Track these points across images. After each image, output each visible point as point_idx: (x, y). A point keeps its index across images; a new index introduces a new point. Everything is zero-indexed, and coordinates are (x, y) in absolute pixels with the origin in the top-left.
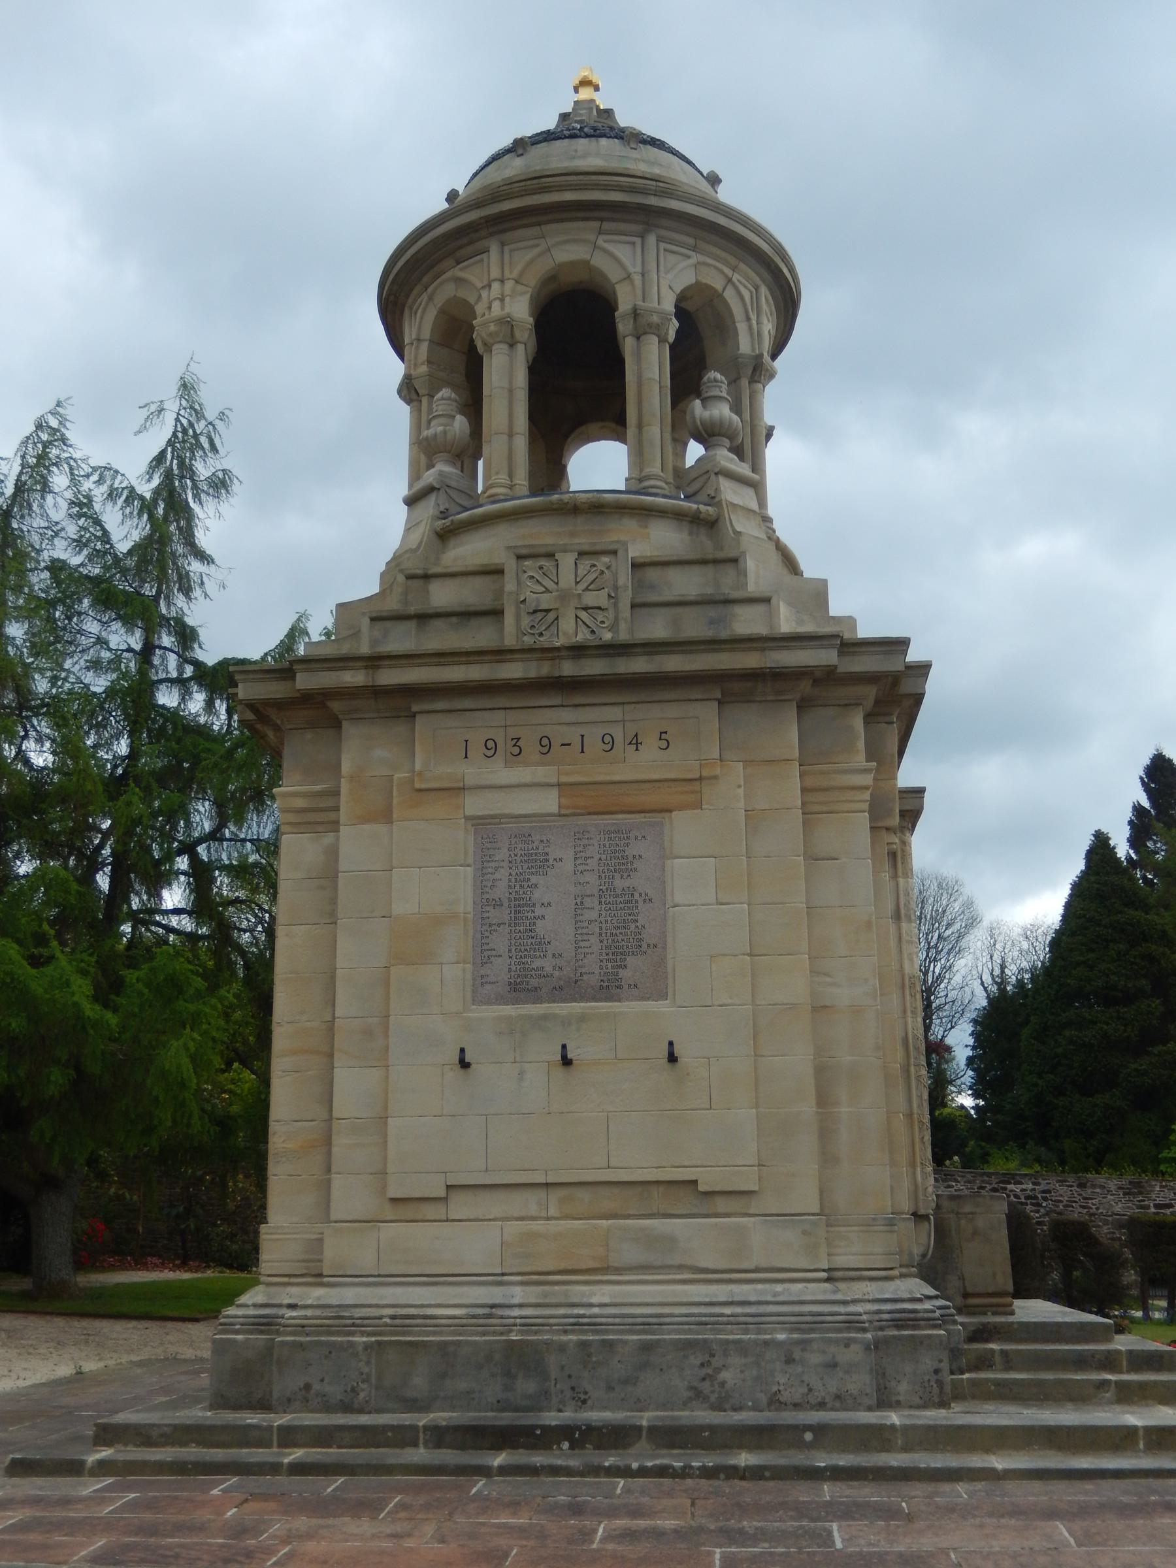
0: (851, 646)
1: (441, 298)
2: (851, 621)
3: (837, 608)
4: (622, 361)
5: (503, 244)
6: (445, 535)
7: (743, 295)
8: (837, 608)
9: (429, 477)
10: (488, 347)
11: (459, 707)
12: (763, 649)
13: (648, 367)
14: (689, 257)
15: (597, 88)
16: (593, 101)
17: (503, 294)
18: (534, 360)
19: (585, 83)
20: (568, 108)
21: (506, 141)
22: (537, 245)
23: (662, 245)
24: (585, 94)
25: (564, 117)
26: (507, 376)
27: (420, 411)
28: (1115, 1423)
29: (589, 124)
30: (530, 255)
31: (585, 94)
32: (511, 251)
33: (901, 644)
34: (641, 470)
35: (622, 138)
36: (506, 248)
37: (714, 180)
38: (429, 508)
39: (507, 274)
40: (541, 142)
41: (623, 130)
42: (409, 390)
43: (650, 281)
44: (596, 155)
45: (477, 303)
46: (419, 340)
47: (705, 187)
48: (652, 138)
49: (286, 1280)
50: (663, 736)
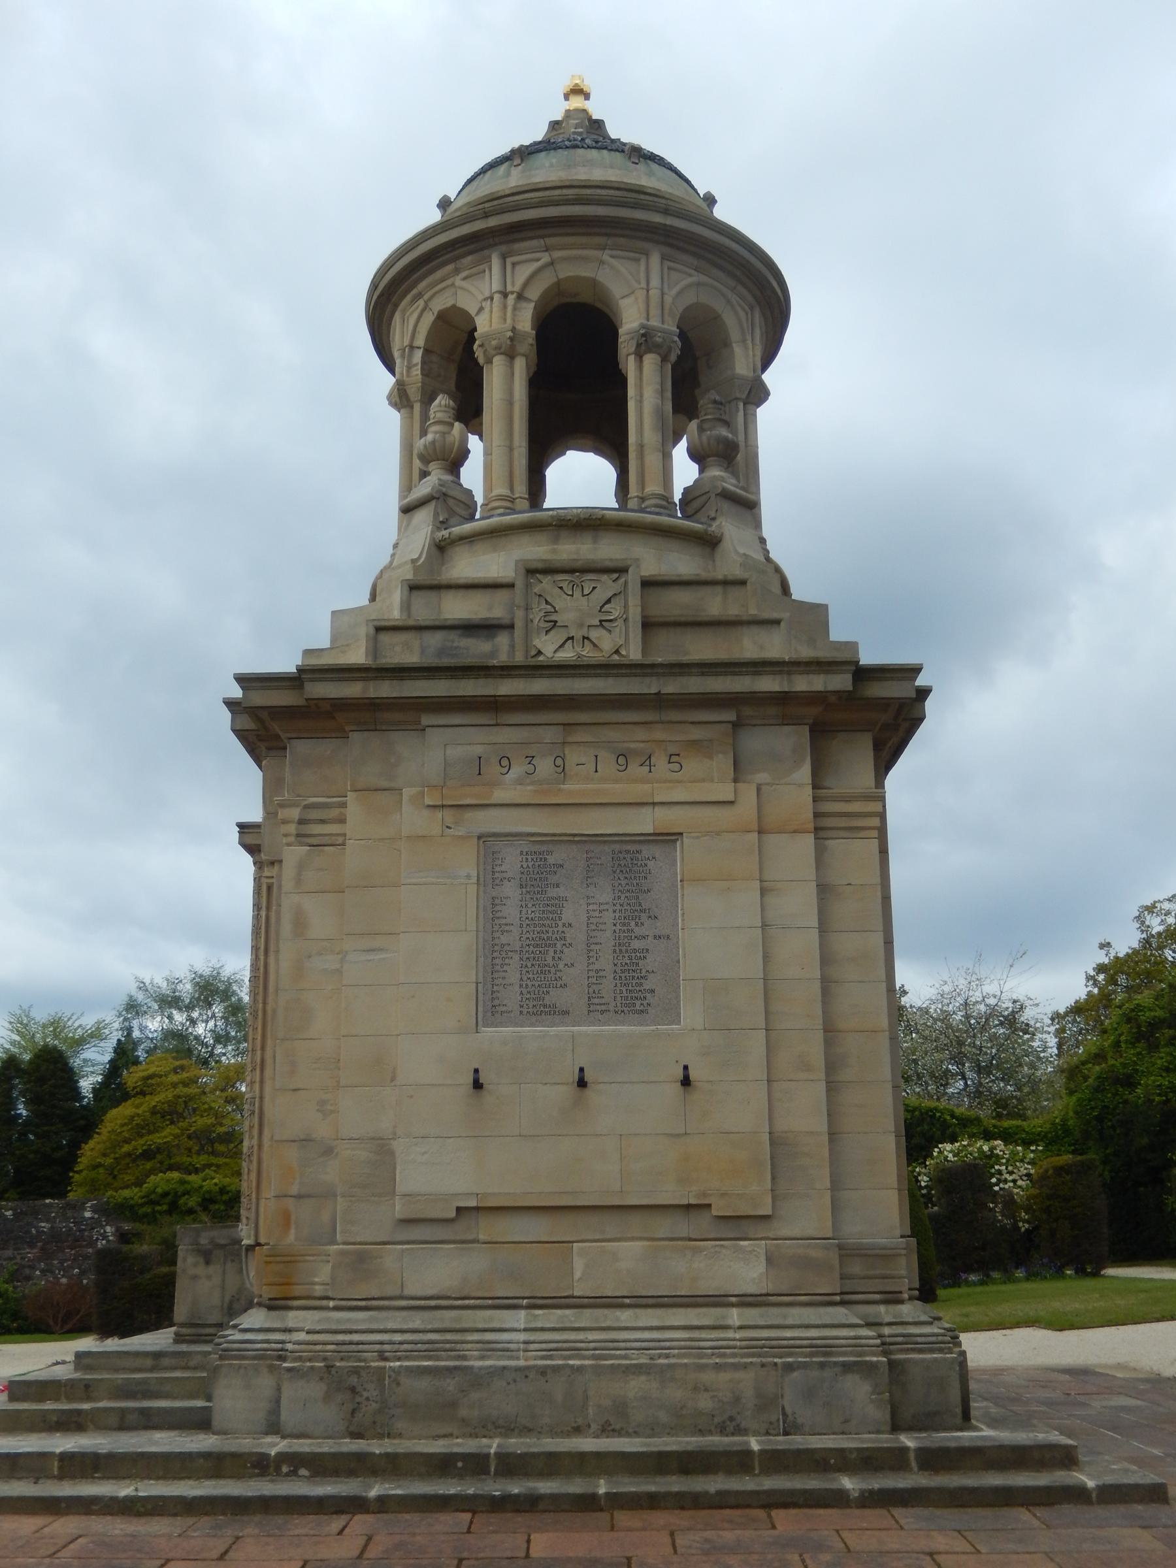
0: (863, 674)
1: (440, 303)
2: (853, 646)
3: (837, 634)
4: (626, 379)
5: (504, 258)
6: (441, 548)
7: (737, 321)
8: (837, 634)
9: (424, 488)
10: (489, 361)
11: (436, 723)
12: (789, 673)
13: (645, 388)
14: (690, 275)
15: (587, 96)
16: (585, 111)
17: (497, 303)
18: (535, 373)
19: (577, 91)
20: (558, 116)
21: (503, 149)
22: (538, 260)
23: (667, 263)
24: (577, 102)
25: (554, 125)
26: (505, 387)
27: (412, 418)
28: (743, 1489)
29: (581, 133)
30: (535, 265)
31: (577, 102)
32: (514, 264)
33: (916, 670)
34: (643, 489)
35: (623, 151)
36: (509, 261)
37: (710, 200)
38: (423, 517)
39: (509, 288)
40: (541, 151)
41: (613, 141)
42: (400, 398)
43: (641, 298)
44: (597, 169)
45: (477, 314)
46: (412, 347)
47: (704, 205)
48: (662, 159)
49: (363, 1303)
50: (674, 759)
